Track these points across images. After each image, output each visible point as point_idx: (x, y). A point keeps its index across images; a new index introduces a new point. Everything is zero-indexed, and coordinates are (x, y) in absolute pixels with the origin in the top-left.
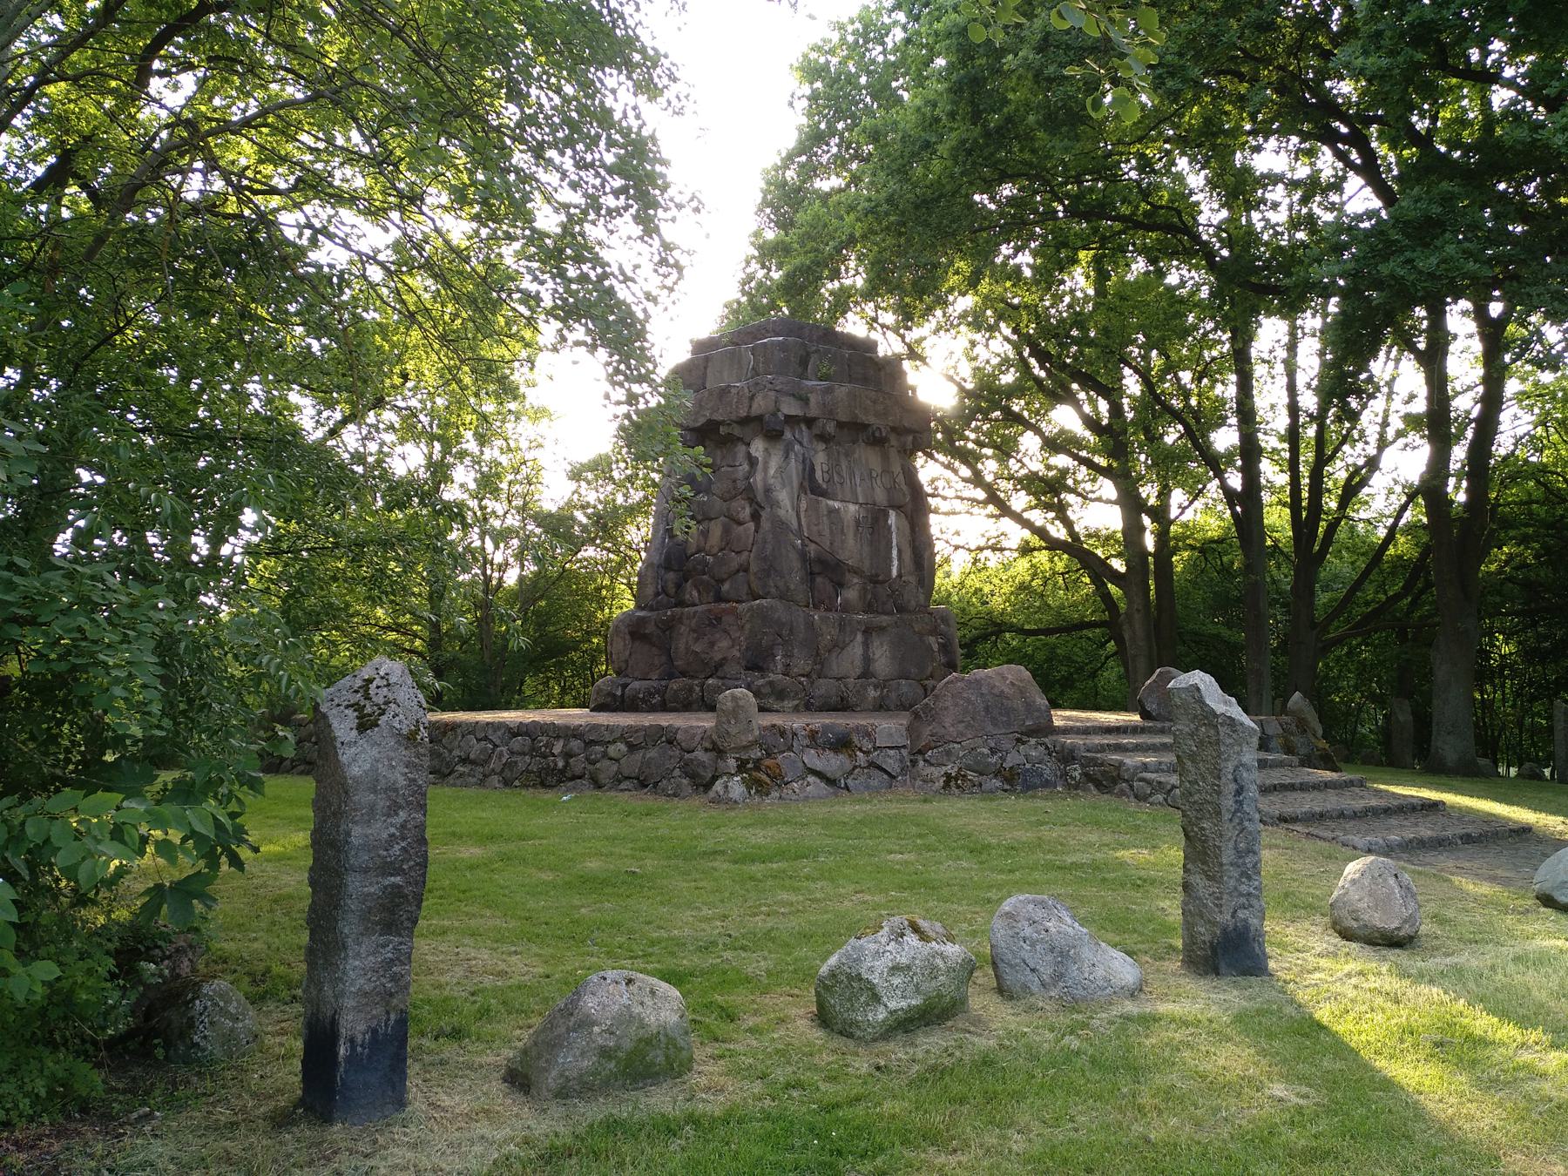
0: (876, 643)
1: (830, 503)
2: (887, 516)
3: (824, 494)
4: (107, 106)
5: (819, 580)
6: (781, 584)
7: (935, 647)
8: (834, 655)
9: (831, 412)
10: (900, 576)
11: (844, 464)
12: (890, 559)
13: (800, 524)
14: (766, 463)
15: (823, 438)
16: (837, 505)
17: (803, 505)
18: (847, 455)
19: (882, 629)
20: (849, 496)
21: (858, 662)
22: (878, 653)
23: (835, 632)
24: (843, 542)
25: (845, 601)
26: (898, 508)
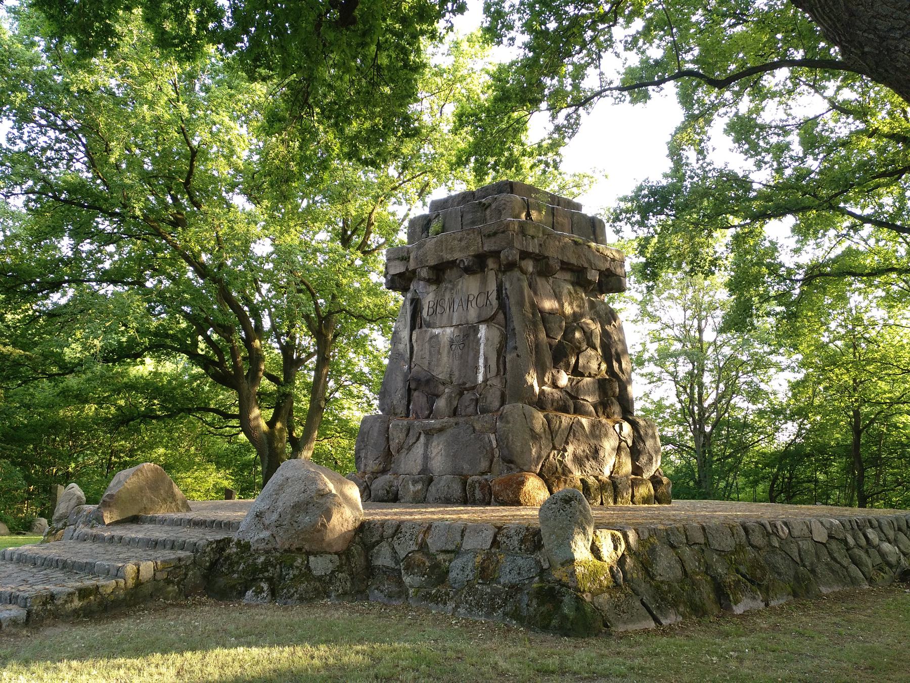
2: (476, 330)
3: (429, 325)
4: (93, 277)
5: (416, 394)
10: (486, 380)
12: (477, 368)
15: (429, 281)
16: (437, 331)
17: (414, 338)
19: (441, 430)
21: (419, 461)
22: (435, 452)
23: (402, 436)
24: (438, 360)
26: (487, 321)
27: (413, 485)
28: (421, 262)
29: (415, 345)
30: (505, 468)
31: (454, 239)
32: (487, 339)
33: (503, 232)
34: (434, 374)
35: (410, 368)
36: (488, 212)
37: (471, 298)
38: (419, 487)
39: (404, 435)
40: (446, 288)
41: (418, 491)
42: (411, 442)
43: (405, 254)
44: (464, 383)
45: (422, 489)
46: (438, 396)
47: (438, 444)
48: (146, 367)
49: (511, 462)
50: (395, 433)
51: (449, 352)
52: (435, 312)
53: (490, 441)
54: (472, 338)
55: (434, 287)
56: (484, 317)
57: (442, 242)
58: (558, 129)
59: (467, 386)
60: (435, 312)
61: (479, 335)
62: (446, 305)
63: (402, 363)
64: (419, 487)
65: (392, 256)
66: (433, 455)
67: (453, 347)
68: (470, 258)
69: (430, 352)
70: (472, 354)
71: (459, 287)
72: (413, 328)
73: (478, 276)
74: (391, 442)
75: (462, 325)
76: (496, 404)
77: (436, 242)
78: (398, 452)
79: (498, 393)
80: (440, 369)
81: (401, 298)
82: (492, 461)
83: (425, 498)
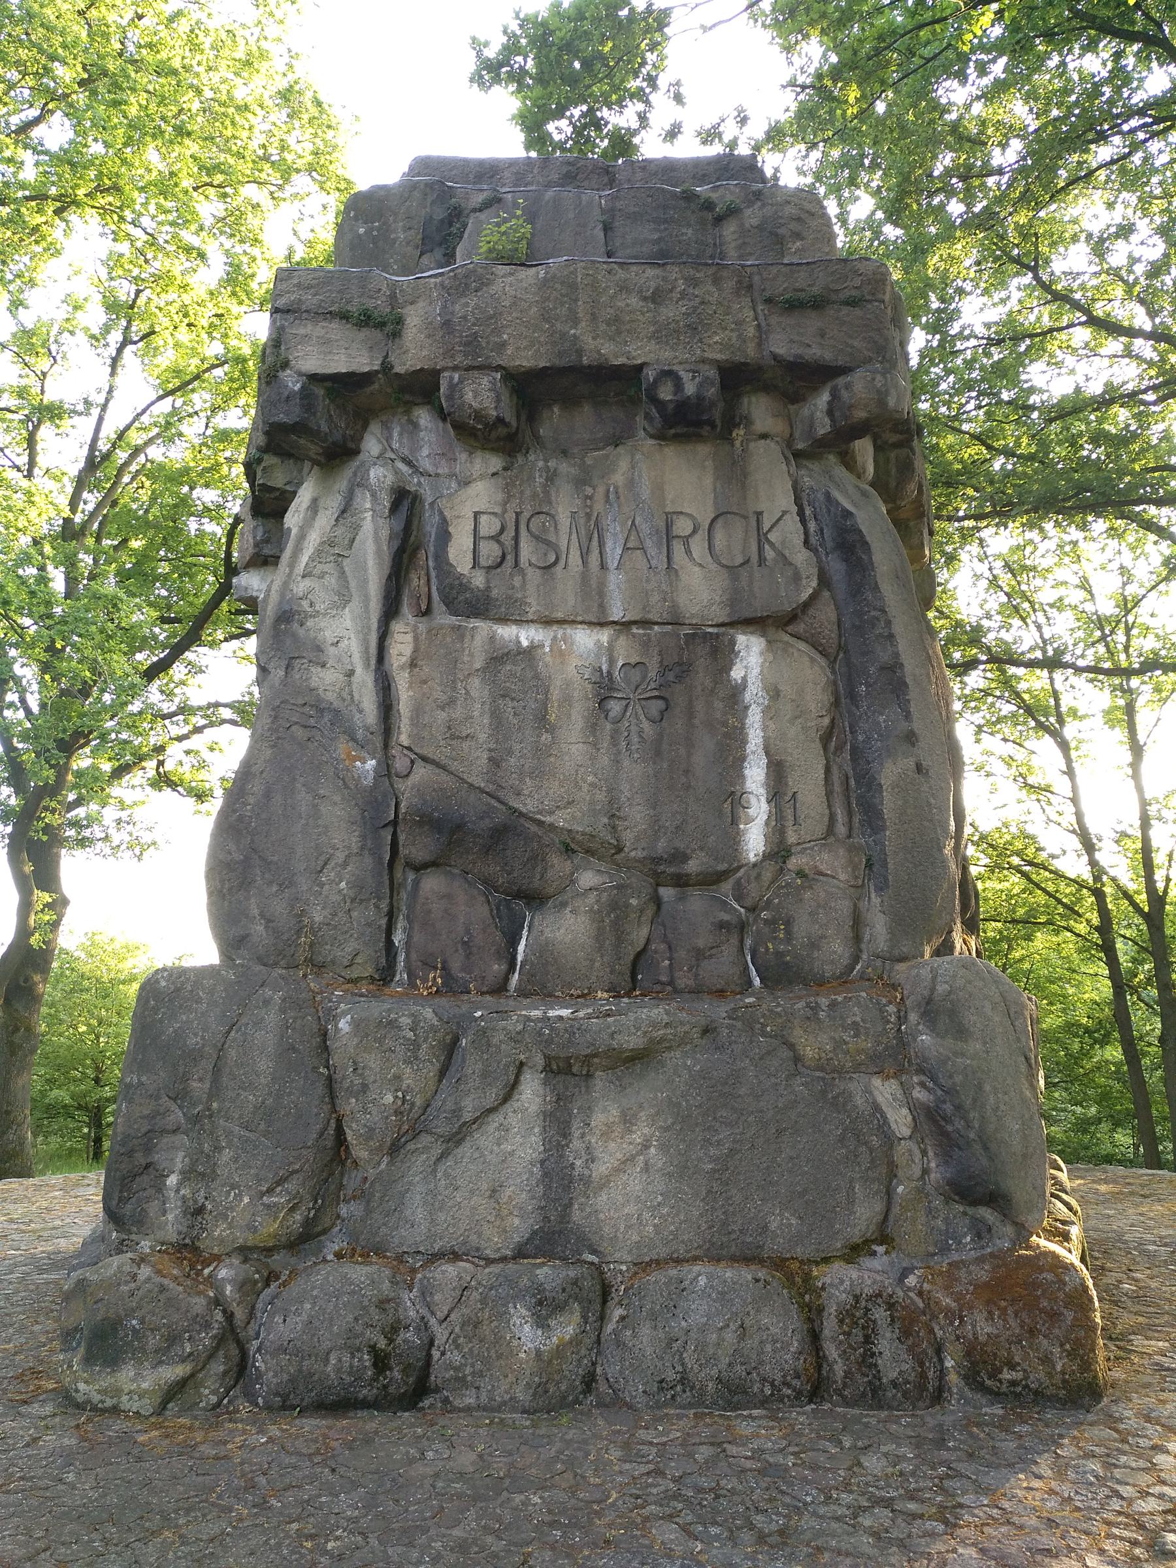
0: (605, 1113)
1: (506, 632)
5: (432, 883)
6: (279, 908)
7: (900, 1121)
8: (417, 1164)
9: (472, 343)
10: (778, 852)
11: (565, 507)
13: (387, 707)
14: (302, 537)
16: (525, 636)
17: (401, 645)
18: (582, 481)
20: (567, 598)
25: (543, 953)
27: (541, 1323)
28: (472, 343)
30: (962, 1225)
31: (624, 288)
32: (774, 693)
33: (852, 303)
34: (527, 805)
35: (386, 771)
36: (729, 230)
37: (683, 527)
38: (566, 1328)
40: (551, 477)
41: (559, 1352)
42: (469, 1107)
43: (379, 305)
44: (680, 857)
45: (575, 1341)
46: (535, 899)
47: (628, 1120)
49: (997, 1199)
50: (372, 1061)
51: (593, 727)
52: (508, 558)
54: (701, 678)
55: (496, 462)
57: (573, 286)
58: (285, 365)
59: (692, 866)
60: (508, 558)
61: (737, 674)
62: (565, 536)
63: (342, 747)
64: (566, 1328)
65: (311, 300)
66: (600, 1169)
67: (615, 707)
68: (712, 373)
69: (497, 717)
70: (706, 744)
71: (618, 478)
72: (390, 611)
73: (703, 450)
74: (350, 1105)
75: (645, 623)
76: (837, 948)
77: (545, 283)
78: (395, 1149)
79: (844, 906)
80: (554, 789)
81: (305, 496)
82: (889, 1193)
83: (589, 1381)
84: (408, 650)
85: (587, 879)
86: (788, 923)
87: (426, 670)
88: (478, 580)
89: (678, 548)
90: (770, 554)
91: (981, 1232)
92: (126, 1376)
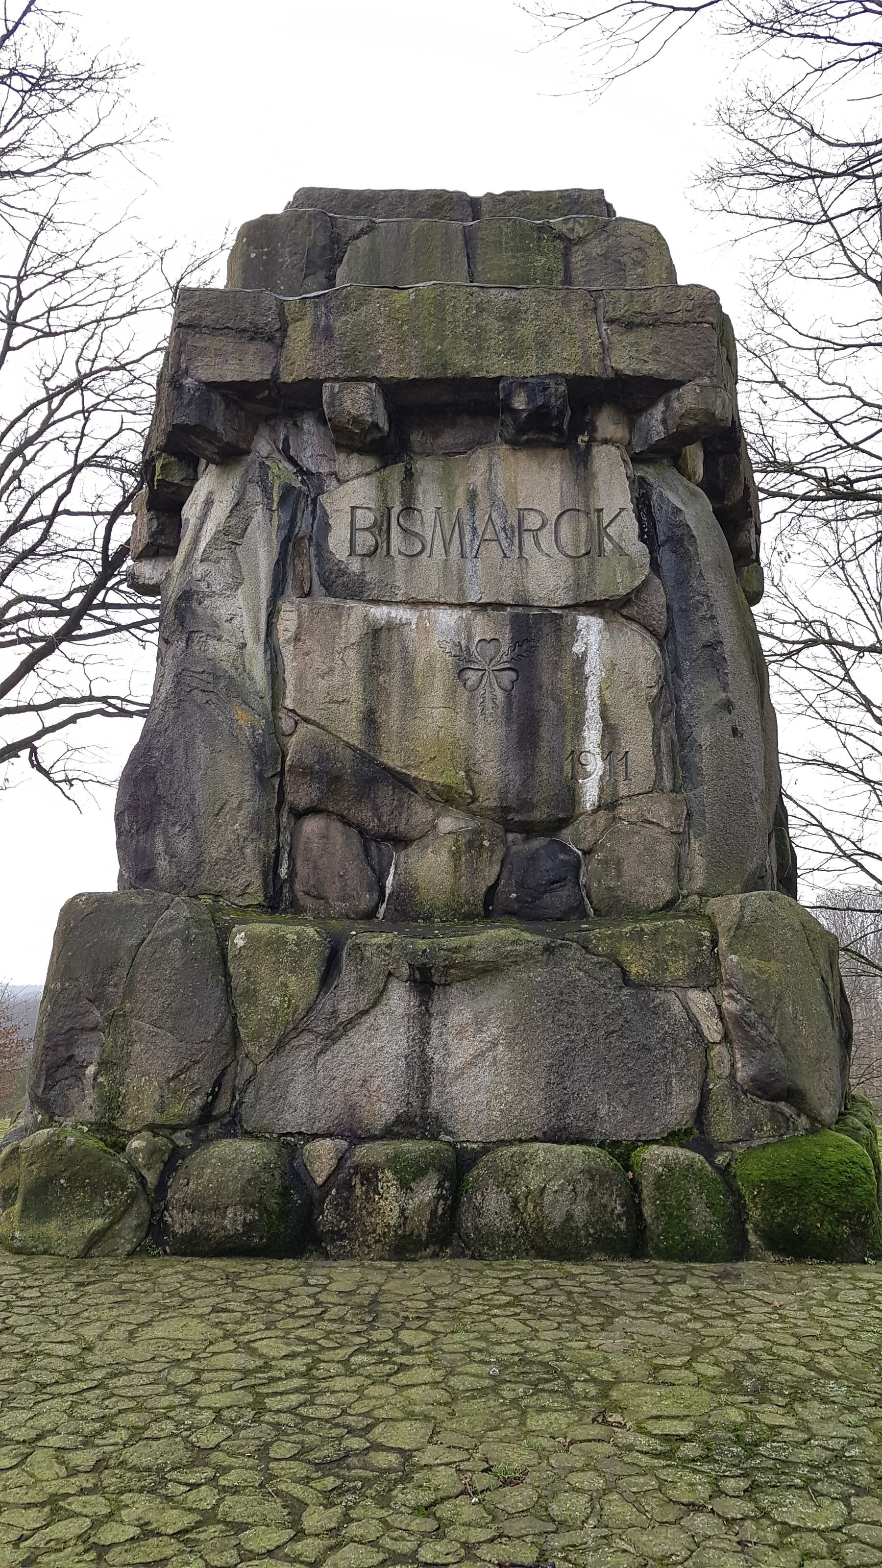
29: (287, 652)
32: (611, 667)
39: (314, 980)
42: (345, 1008)
43: (271, 320)
46: (402, 841)
47: (479, 1023)
48: (837, 487)
53: (692, 1019)
55: (370, 463)
56: (598, 592)
66: (454, 1063)
67: (472, 677)
78: (279, 1047)
79: (666, 849)
84: (292, 626)
85: (447, 824)
86: (618, 863)
87: (309, 643)
88: (355, 566)
89: (528, 539)
90: (608, 545)
91: (783, 1123)
92: (53, 1228)
